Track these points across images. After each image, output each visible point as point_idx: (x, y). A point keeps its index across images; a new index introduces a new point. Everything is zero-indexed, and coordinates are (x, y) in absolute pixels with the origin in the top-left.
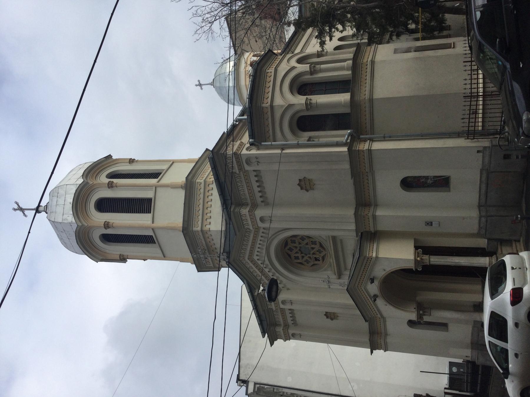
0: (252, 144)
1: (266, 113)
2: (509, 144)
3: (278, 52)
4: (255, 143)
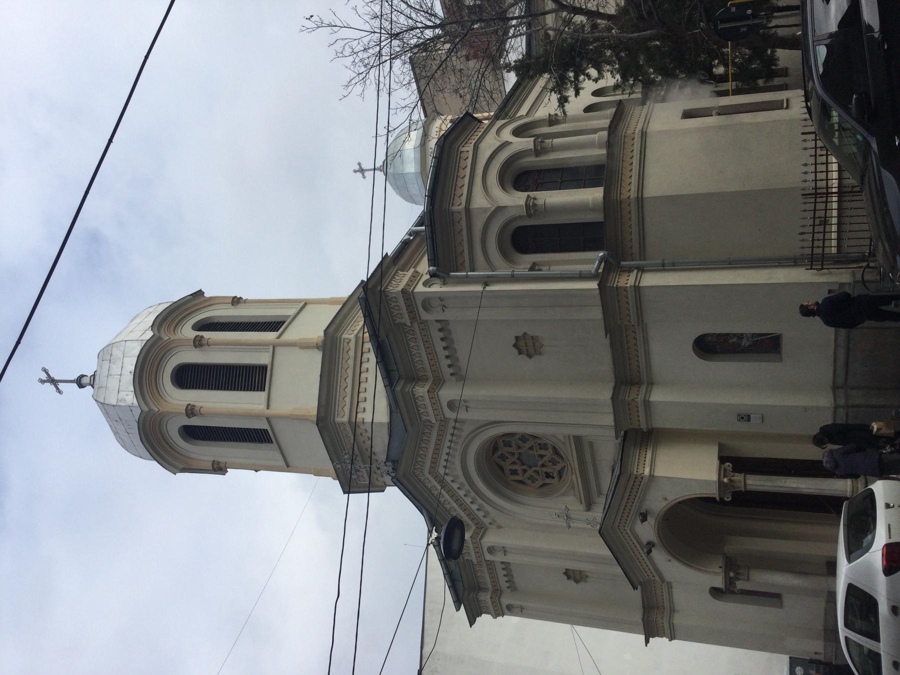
0: (433, 275)
1: (459, 222)
2: (881, 279)
3: (483, 116)
4: (440, 273)
